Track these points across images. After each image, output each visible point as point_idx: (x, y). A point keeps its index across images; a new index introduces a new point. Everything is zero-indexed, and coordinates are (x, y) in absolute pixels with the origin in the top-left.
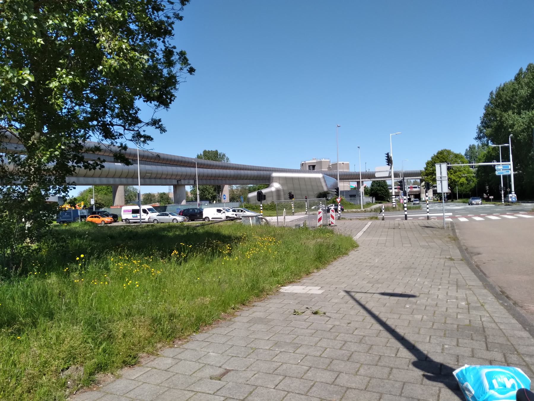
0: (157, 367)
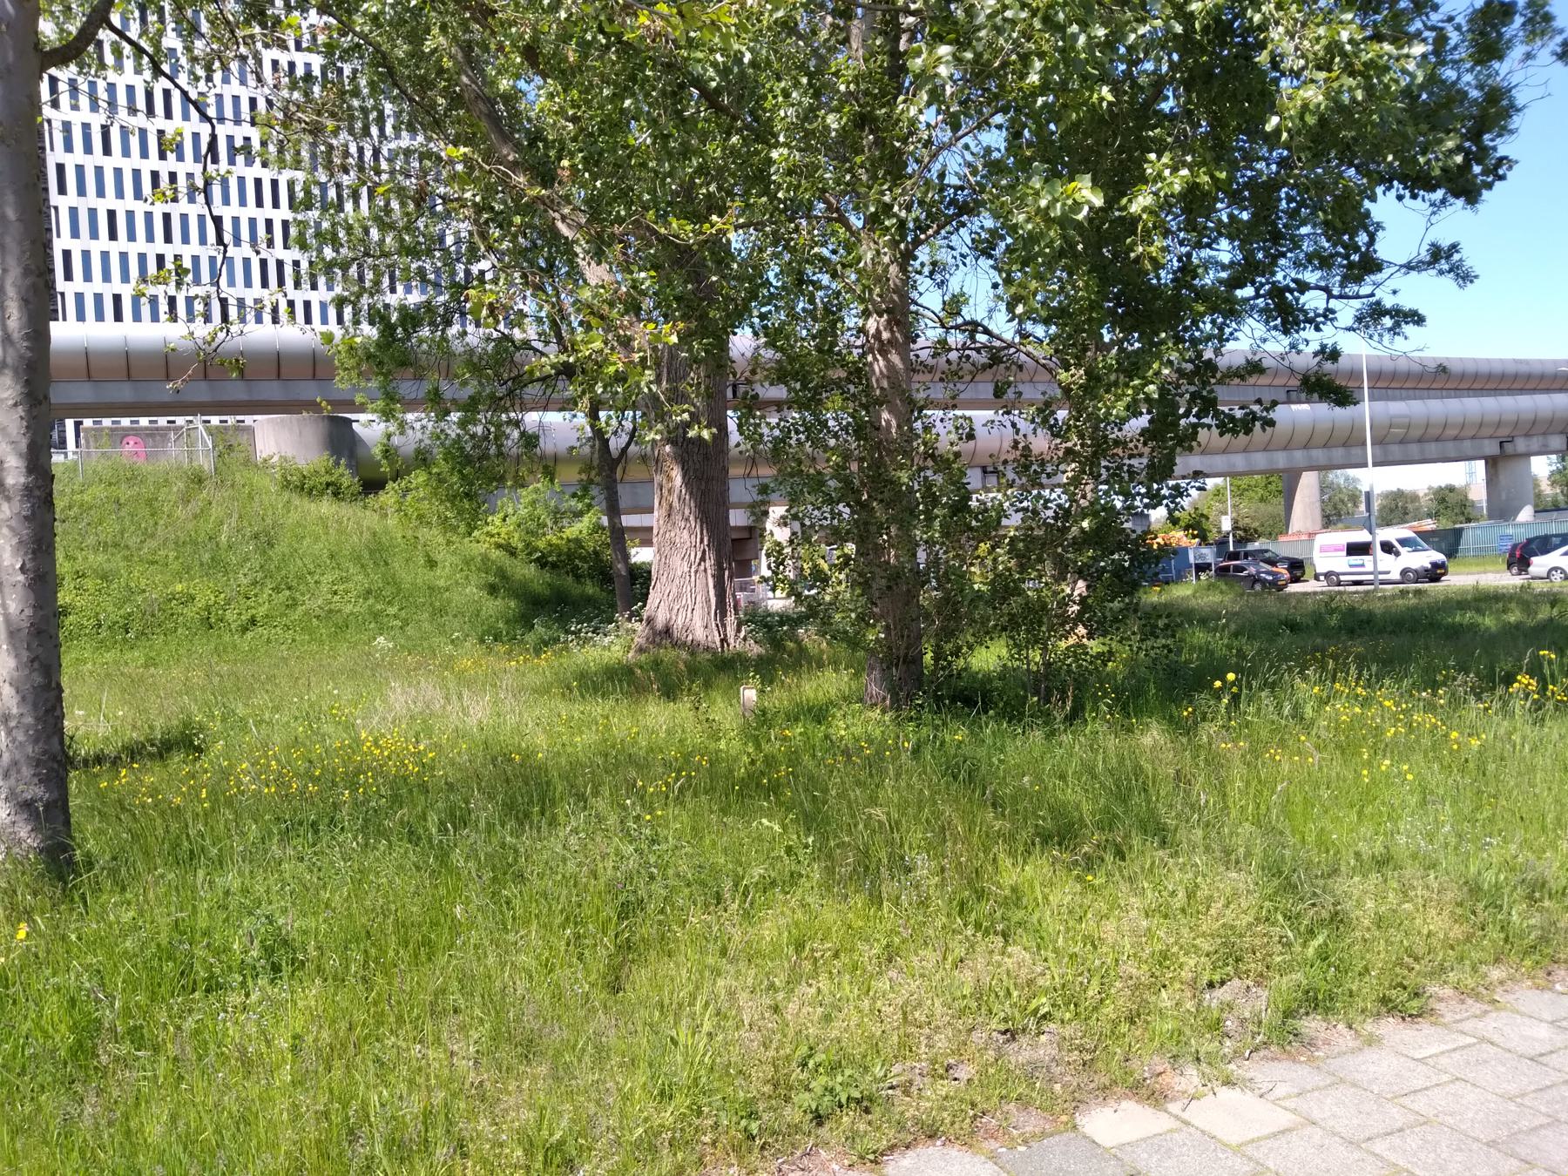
0: (1496, 1038)
